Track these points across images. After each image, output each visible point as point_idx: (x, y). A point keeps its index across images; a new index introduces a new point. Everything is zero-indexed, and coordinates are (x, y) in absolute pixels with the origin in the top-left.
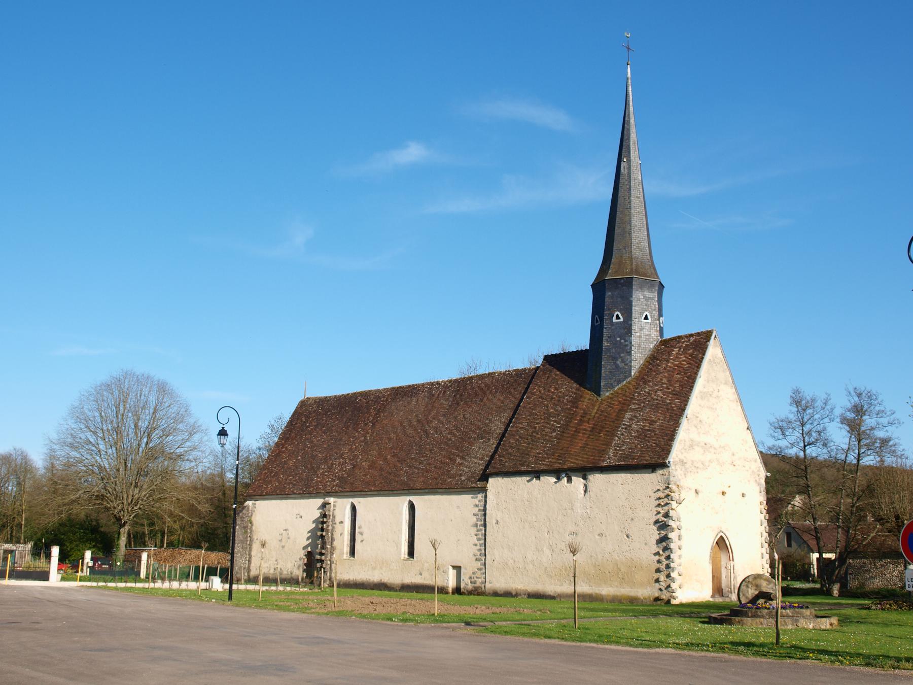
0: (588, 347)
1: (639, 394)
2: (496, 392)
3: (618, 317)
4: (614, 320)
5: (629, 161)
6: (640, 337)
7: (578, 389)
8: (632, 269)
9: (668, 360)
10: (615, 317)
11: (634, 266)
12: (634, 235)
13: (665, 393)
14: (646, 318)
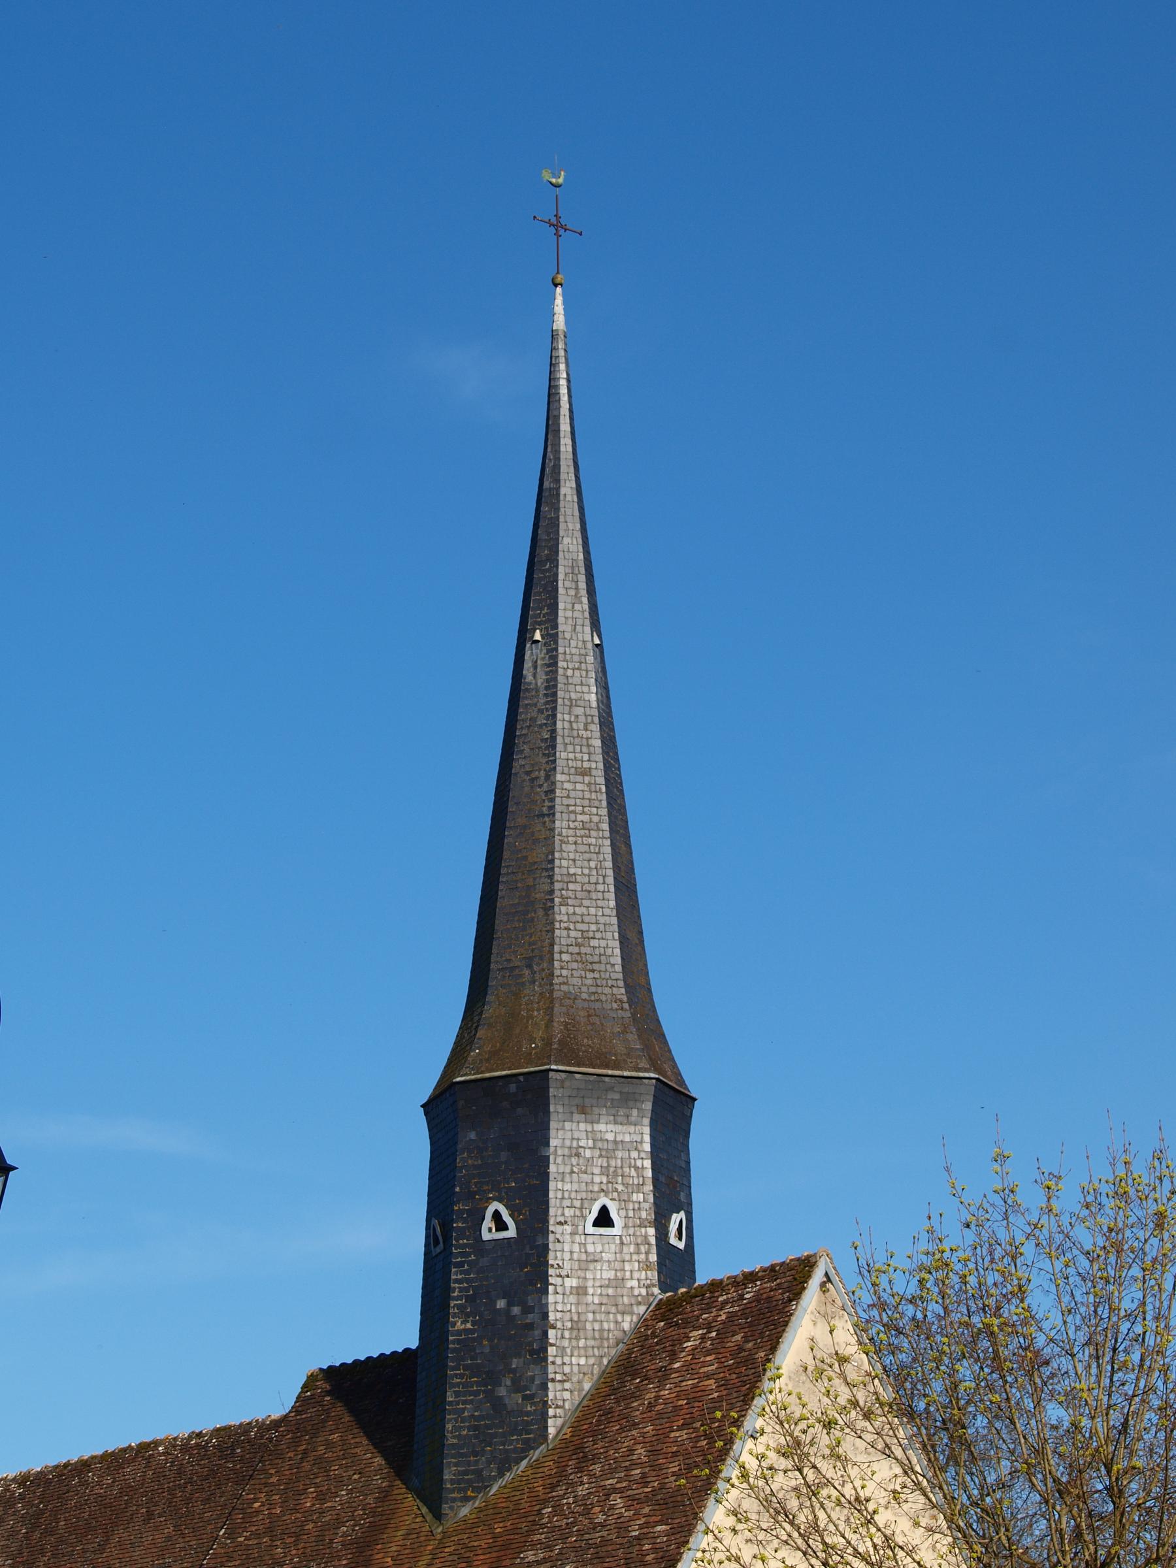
0: (414, 1344)
1: (558, 1510)
2: (150, 1515)
3: (501, 1226)
4: (488, 1232)
5: (552, 638)
6: (581, 1291)
7: (385, 1495)
8: (548, 1042)
9: (664, 1375)
10: (488, 1223)
11: (557, 1028)
12: (561, 913)
13: (633, 1501)
14: (604, 1220)
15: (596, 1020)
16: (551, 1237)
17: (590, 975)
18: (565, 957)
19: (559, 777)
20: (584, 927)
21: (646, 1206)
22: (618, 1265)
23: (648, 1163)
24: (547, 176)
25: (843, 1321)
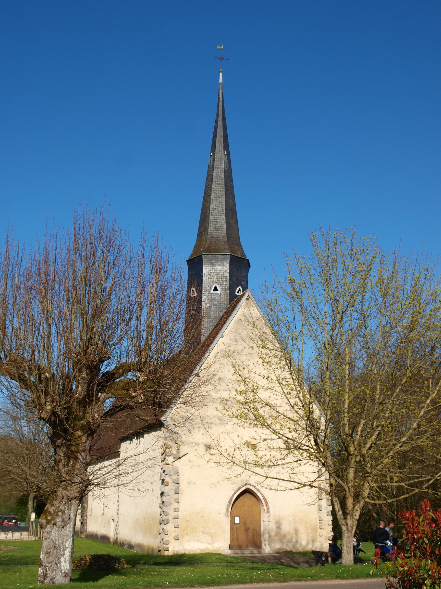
12: (211, 218)
14: (216, 289)
15: (217, 242)
16: (203, 295)
17: (217, 232)
18: (211, 228)
19: (213, 186)
20: (217, 220)
21: (227, 285)
22: (219, 300)
23: (228, 275)
24: (218, 47)
25: (253, 308)
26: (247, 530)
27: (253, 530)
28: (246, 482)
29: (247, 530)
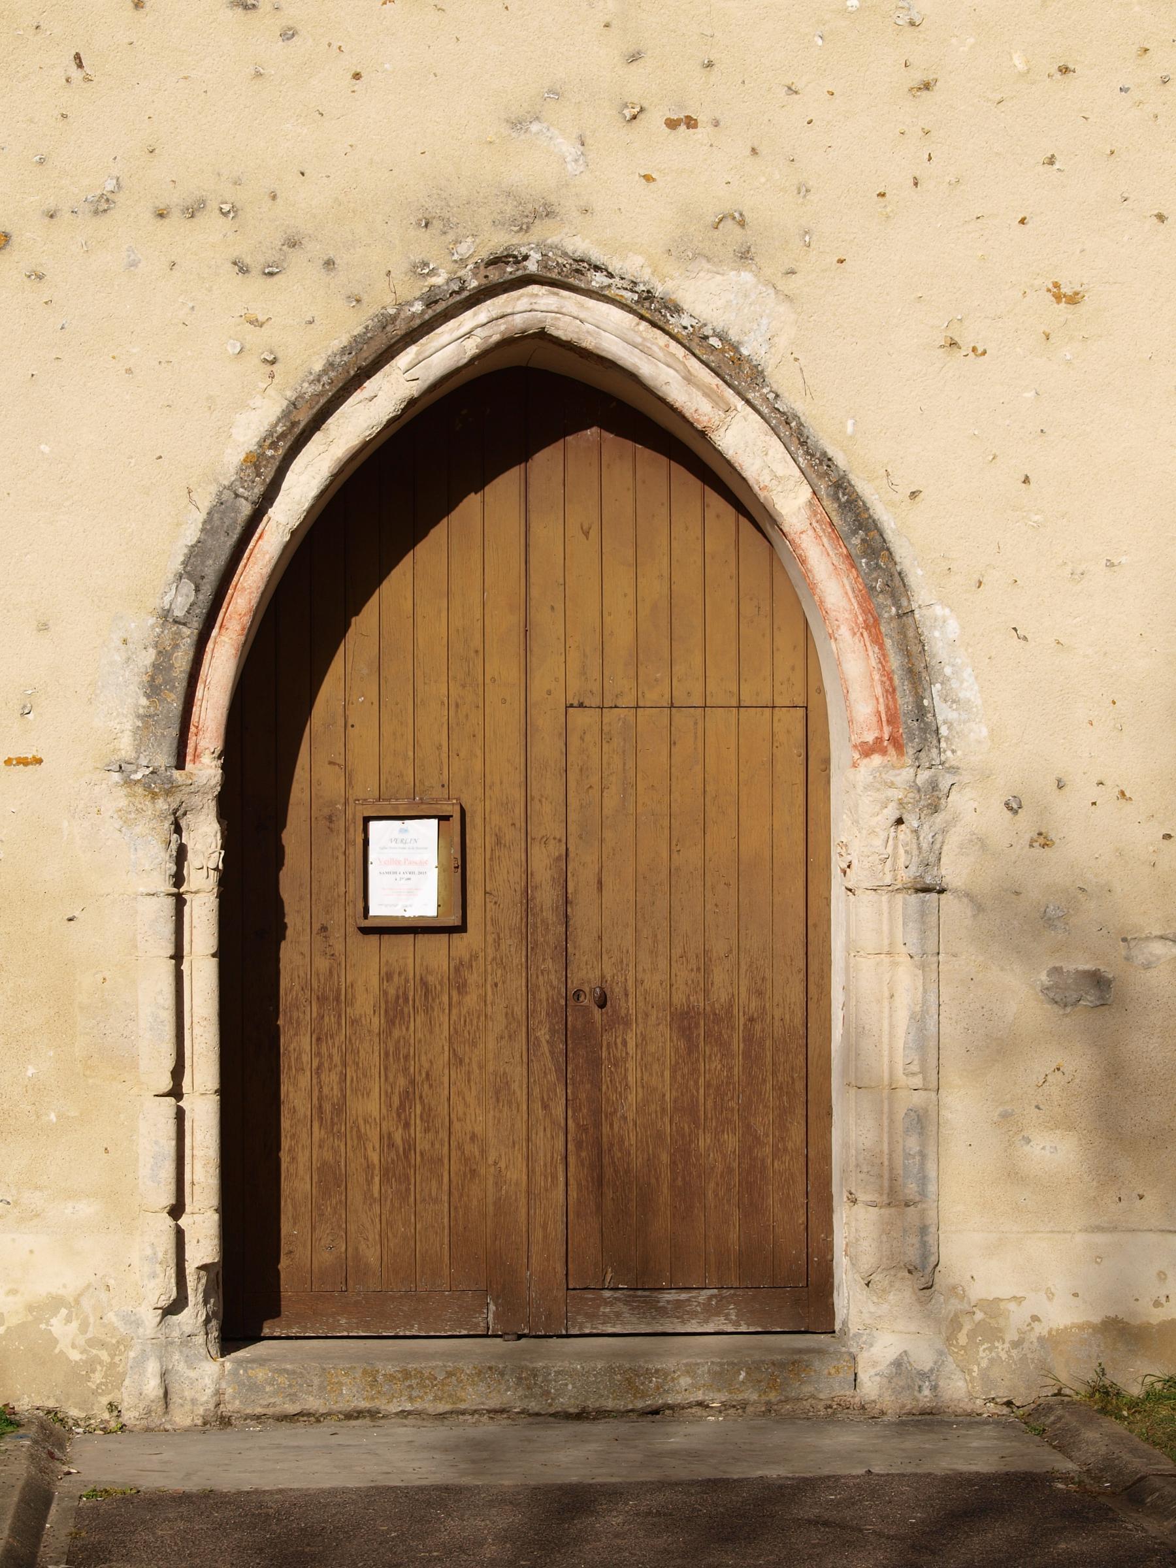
26: (581, 1025)
27: (684, 1021)
28: (498, 241)
29: (581, 1025)
